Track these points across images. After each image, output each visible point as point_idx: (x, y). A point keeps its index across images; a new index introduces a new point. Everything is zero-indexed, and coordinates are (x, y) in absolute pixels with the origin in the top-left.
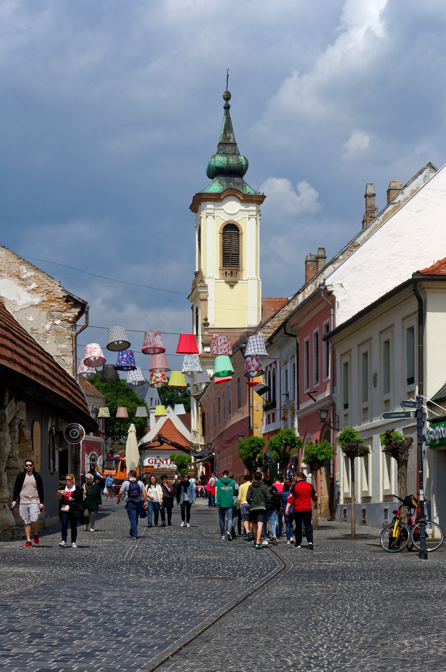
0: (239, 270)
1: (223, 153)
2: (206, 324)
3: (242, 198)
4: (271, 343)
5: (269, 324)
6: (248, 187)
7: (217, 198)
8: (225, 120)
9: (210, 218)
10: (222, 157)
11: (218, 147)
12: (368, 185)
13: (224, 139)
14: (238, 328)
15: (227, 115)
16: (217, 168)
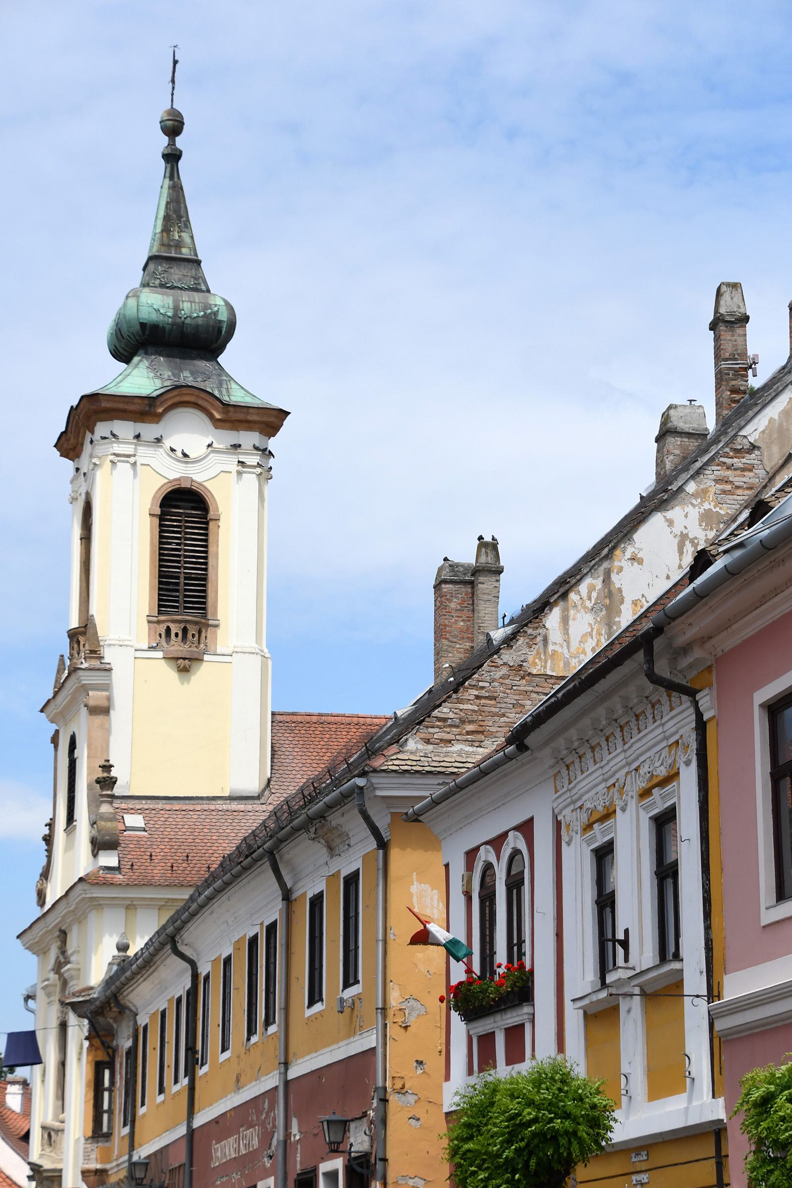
0: (208, 626)
1: (162, 286)
2: (106, 782)
3: (218, 416)
4: (522, 748)
5: (444, 711)
6: (234, 386)
7: (144, 410)
8: (165, 191)
9: (124, 468)
10: (159, 297)
11: (144, 269)
12: (724, 288)
13: (162, 245)
14: (202, 798)
15: (171, 178)
16: (143, 325)
